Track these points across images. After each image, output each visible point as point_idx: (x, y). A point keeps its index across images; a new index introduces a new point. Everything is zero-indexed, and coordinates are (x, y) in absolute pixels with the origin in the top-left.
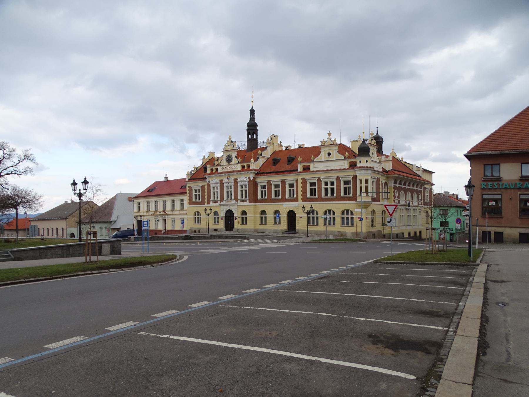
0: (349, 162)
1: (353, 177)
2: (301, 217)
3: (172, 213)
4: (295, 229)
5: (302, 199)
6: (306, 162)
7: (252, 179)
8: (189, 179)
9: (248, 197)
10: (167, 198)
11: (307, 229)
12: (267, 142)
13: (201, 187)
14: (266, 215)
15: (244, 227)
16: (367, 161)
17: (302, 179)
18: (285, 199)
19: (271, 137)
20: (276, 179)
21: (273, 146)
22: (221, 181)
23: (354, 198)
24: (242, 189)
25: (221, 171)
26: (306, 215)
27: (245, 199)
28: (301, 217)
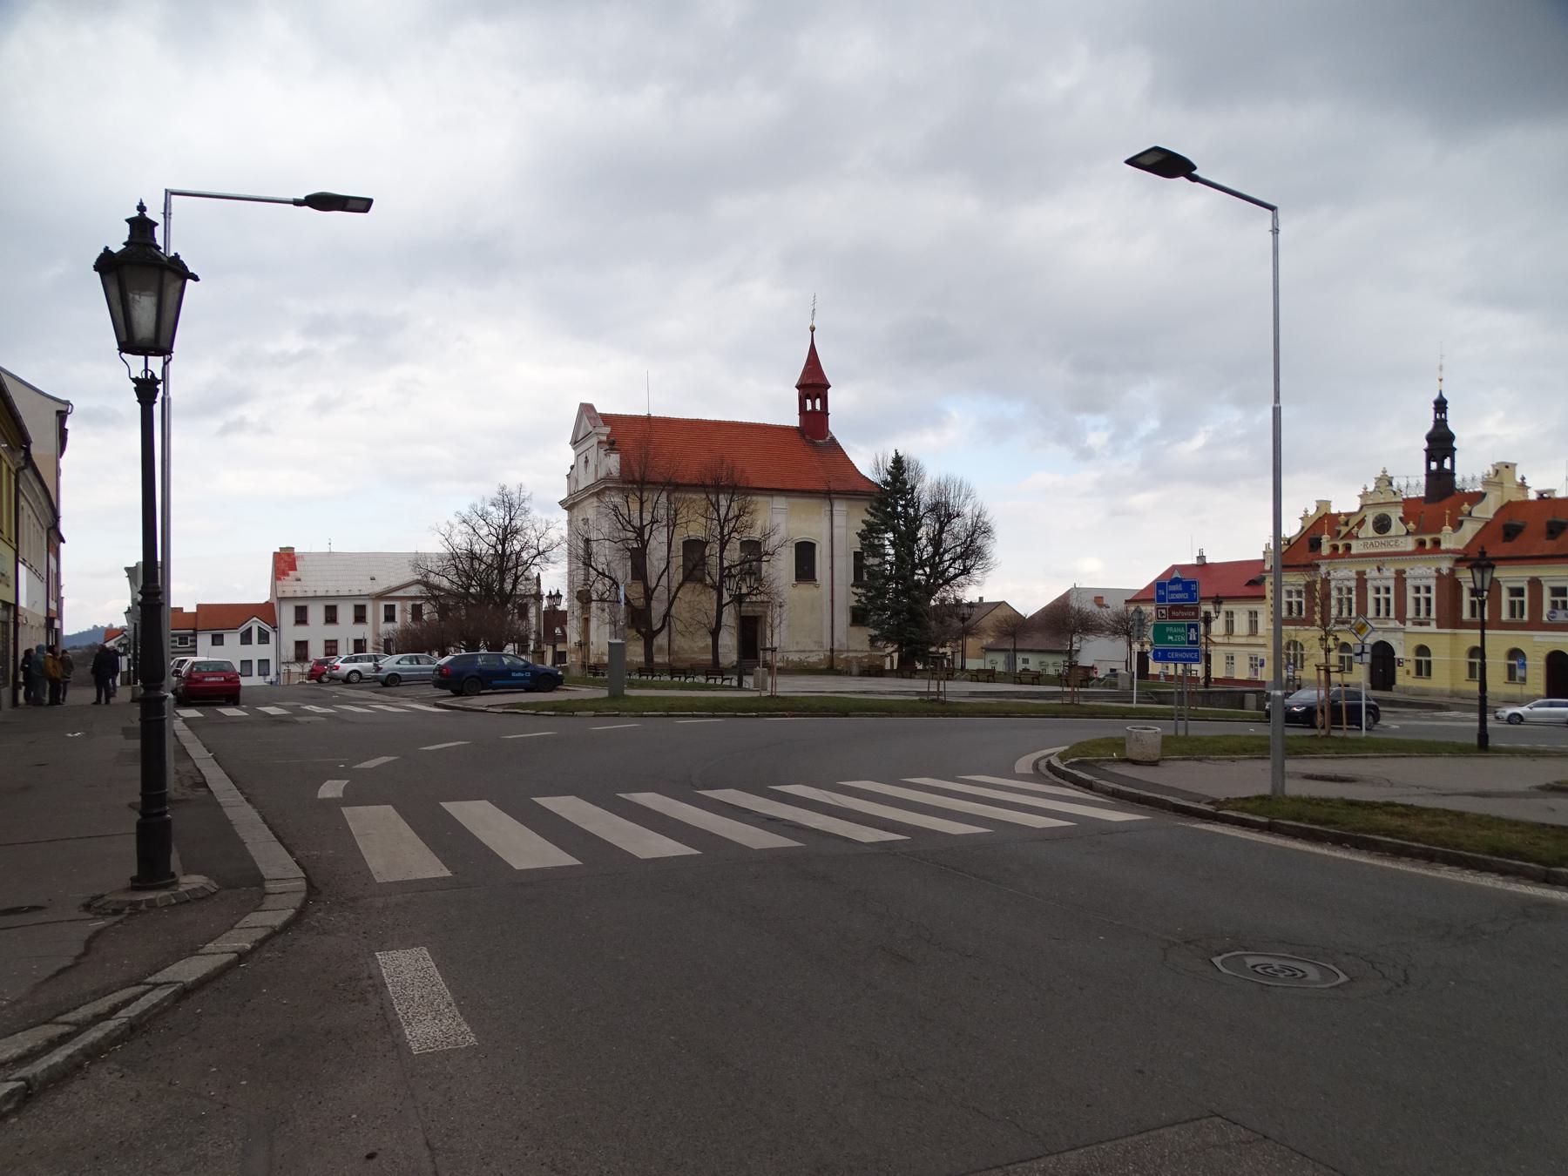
3: (1226, 641)
7: (1445, 571)
9: (1433, 615)
10: (1238, 607)
12: (1486, 483)
13: (1529, 582)
15: (1422, 683)
19: (1497, 468)
21: (1502, 492)
22: (1361, 575)
24: (1418, 595)
27: (1425, 619)
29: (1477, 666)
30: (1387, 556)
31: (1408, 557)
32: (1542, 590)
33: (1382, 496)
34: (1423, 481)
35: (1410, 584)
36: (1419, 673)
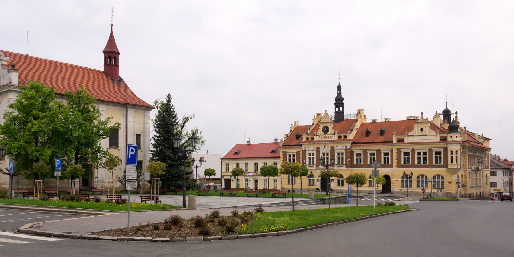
0: (440, 137)
1: (443, 149)
2: (397, 181)
4: (390, 191)
5: (396, 166)
6: (402, 134)
7: (348, 147)
8: (283, 146)
9: (344, 163)
11: (300, 188)
13: (296, 153)
14: (412, 179)
16: (457, 137)
17: (396, 149)
18: (415, 165)
20: (372, 149)
21: (361, 119)
23: (446, 166)
25: (318, 140)
26: (308, 178)
28: (397, 181)
29: (41, 183)
30: (322, 142)
31: (317, 143)
32: (415, 153)
33: (325, 120)
34: (334, 115)
35: (336, 152)
36: (339, 185)
